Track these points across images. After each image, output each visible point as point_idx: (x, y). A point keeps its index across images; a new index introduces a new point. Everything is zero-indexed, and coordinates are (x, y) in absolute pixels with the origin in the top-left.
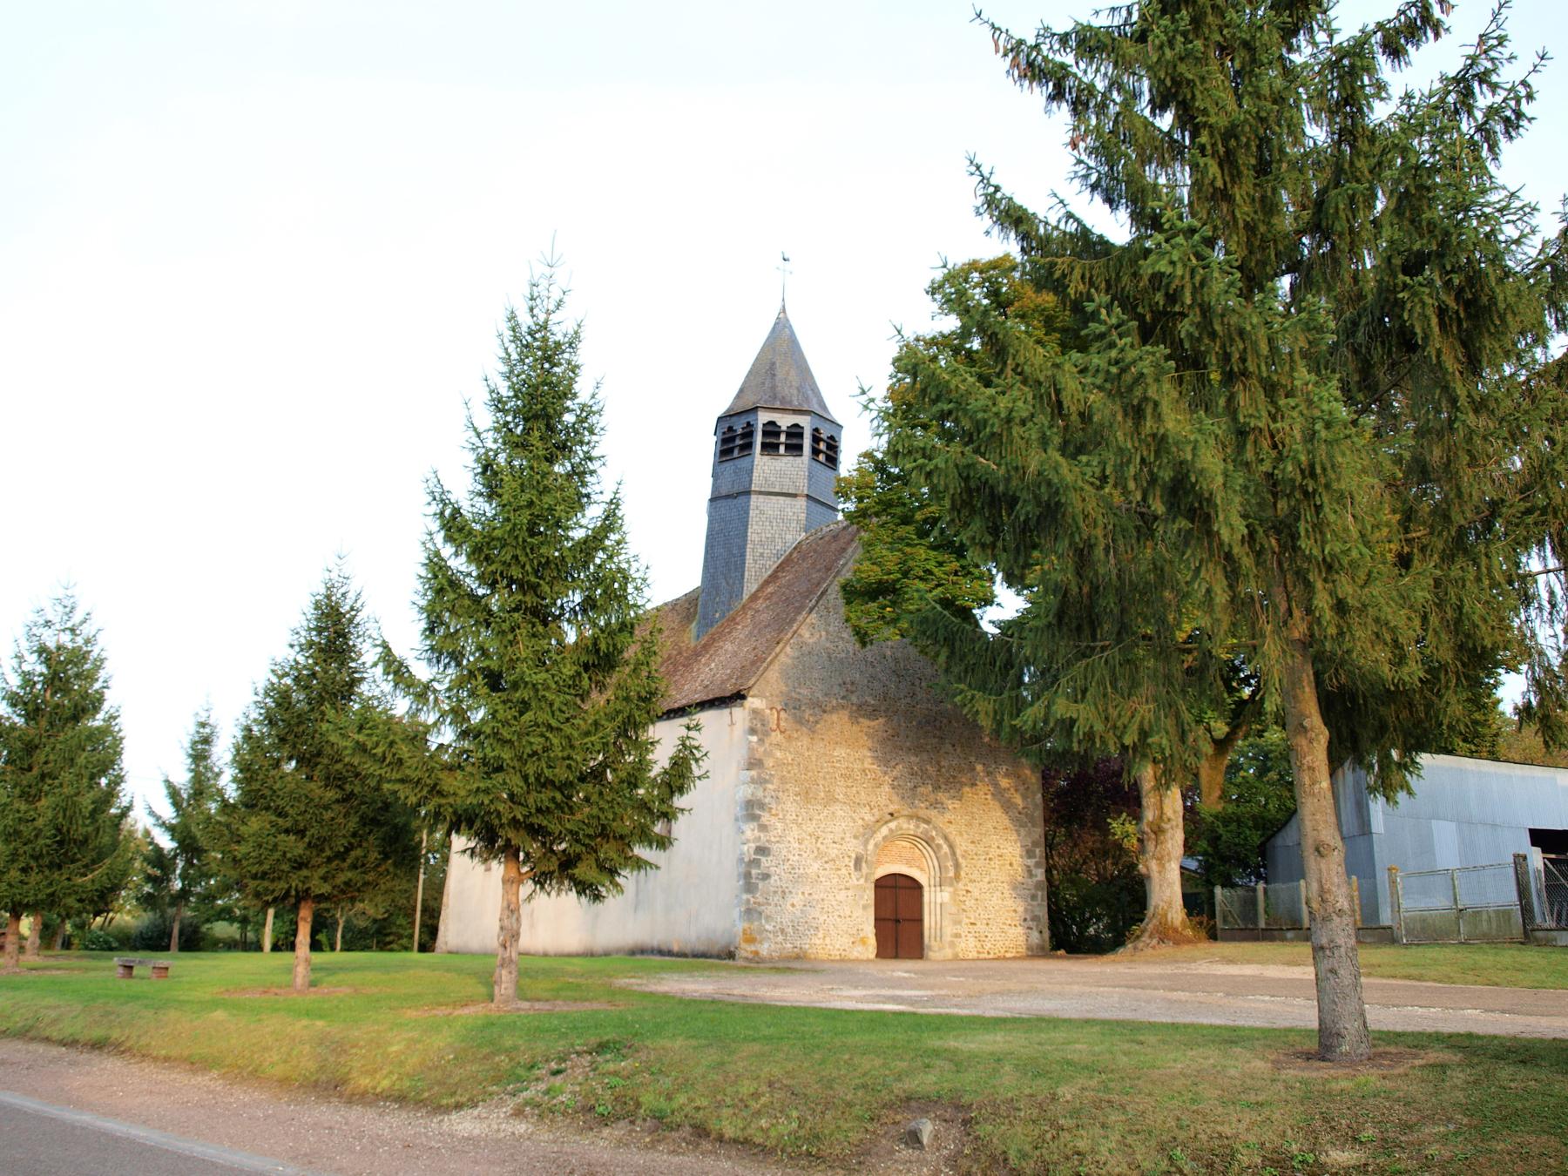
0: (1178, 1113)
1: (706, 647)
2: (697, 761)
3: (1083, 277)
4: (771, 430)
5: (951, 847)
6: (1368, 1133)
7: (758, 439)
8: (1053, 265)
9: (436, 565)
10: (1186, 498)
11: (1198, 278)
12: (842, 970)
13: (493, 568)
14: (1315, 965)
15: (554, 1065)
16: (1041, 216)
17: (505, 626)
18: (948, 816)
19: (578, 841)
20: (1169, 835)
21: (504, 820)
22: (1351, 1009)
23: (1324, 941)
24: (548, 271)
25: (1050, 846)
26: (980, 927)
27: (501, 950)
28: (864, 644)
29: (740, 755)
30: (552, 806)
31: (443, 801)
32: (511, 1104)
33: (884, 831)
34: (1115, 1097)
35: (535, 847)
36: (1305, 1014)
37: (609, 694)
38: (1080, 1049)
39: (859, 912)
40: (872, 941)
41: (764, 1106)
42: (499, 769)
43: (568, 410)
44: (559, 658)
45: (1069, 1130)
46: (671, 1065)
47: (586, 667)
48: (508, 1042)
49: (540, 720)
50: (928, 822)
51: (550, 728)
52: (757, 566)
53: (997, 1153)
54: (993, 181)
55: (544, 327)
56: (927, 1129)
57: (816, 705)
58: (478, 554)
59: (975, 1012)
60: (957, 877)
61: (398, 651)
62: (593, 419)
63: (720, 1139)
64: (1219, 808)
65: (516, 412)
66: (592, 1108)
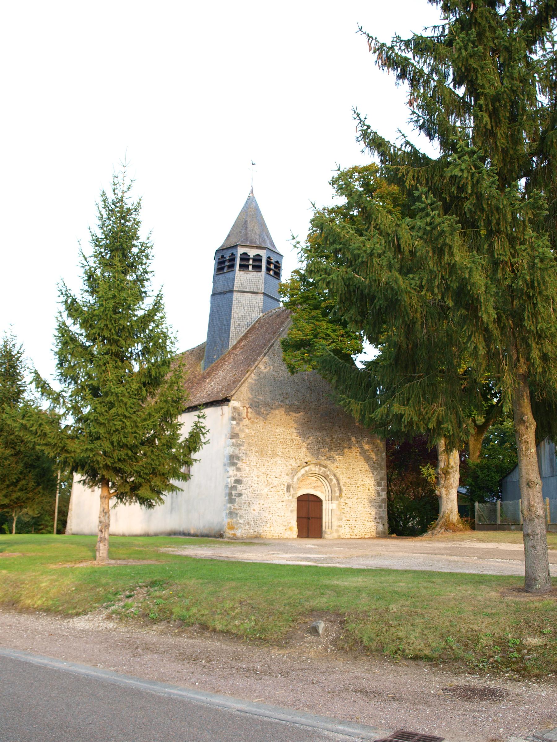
1: (209, 374)
3: (413, 177)
4: (245, 257)
5: (338, 480)
6: (548, 629)
7: (238, 262)
9: (63, 330)
10: (465, 298)
11: (475, 179)
12: (279, 544)
13: (94, 331)
15: (127, 593)
18: (336, 464)
19: (140, 476)
20: (452, 475)
21: (101, 465)
22: (542, 566)
23: (530, 531)
24: (123, 169)
26: (352, 522)
27: (99, 533)
28: (293, 373)
29: (226, 431)
30: (126, 458)
31: (68, 455)
32: (105, 613)
33: (303, 471)
34: (418, 610)
35: (117, 480)
36: (518, 568)
37: (157, 398)
38: (402, 585)
39: (288, 514)
40: (295, 529)
41: (237, 614)
42: (98, 438)
43: (134, 246)
44: (129, 379)
45: (395, 627)
47: (144, 384)
48: (104, 581)
49: (119, 413)
50: (325, 467)
51: (125, 417)
53: (358, 638)
54: (366, 123)
56: (321, 626)
57: (267, 405)
59: (348, 566)
60: (340, 496)
61: (43, 376)
62: (148, 251)
63: (214, 630)
64: (479, 461)
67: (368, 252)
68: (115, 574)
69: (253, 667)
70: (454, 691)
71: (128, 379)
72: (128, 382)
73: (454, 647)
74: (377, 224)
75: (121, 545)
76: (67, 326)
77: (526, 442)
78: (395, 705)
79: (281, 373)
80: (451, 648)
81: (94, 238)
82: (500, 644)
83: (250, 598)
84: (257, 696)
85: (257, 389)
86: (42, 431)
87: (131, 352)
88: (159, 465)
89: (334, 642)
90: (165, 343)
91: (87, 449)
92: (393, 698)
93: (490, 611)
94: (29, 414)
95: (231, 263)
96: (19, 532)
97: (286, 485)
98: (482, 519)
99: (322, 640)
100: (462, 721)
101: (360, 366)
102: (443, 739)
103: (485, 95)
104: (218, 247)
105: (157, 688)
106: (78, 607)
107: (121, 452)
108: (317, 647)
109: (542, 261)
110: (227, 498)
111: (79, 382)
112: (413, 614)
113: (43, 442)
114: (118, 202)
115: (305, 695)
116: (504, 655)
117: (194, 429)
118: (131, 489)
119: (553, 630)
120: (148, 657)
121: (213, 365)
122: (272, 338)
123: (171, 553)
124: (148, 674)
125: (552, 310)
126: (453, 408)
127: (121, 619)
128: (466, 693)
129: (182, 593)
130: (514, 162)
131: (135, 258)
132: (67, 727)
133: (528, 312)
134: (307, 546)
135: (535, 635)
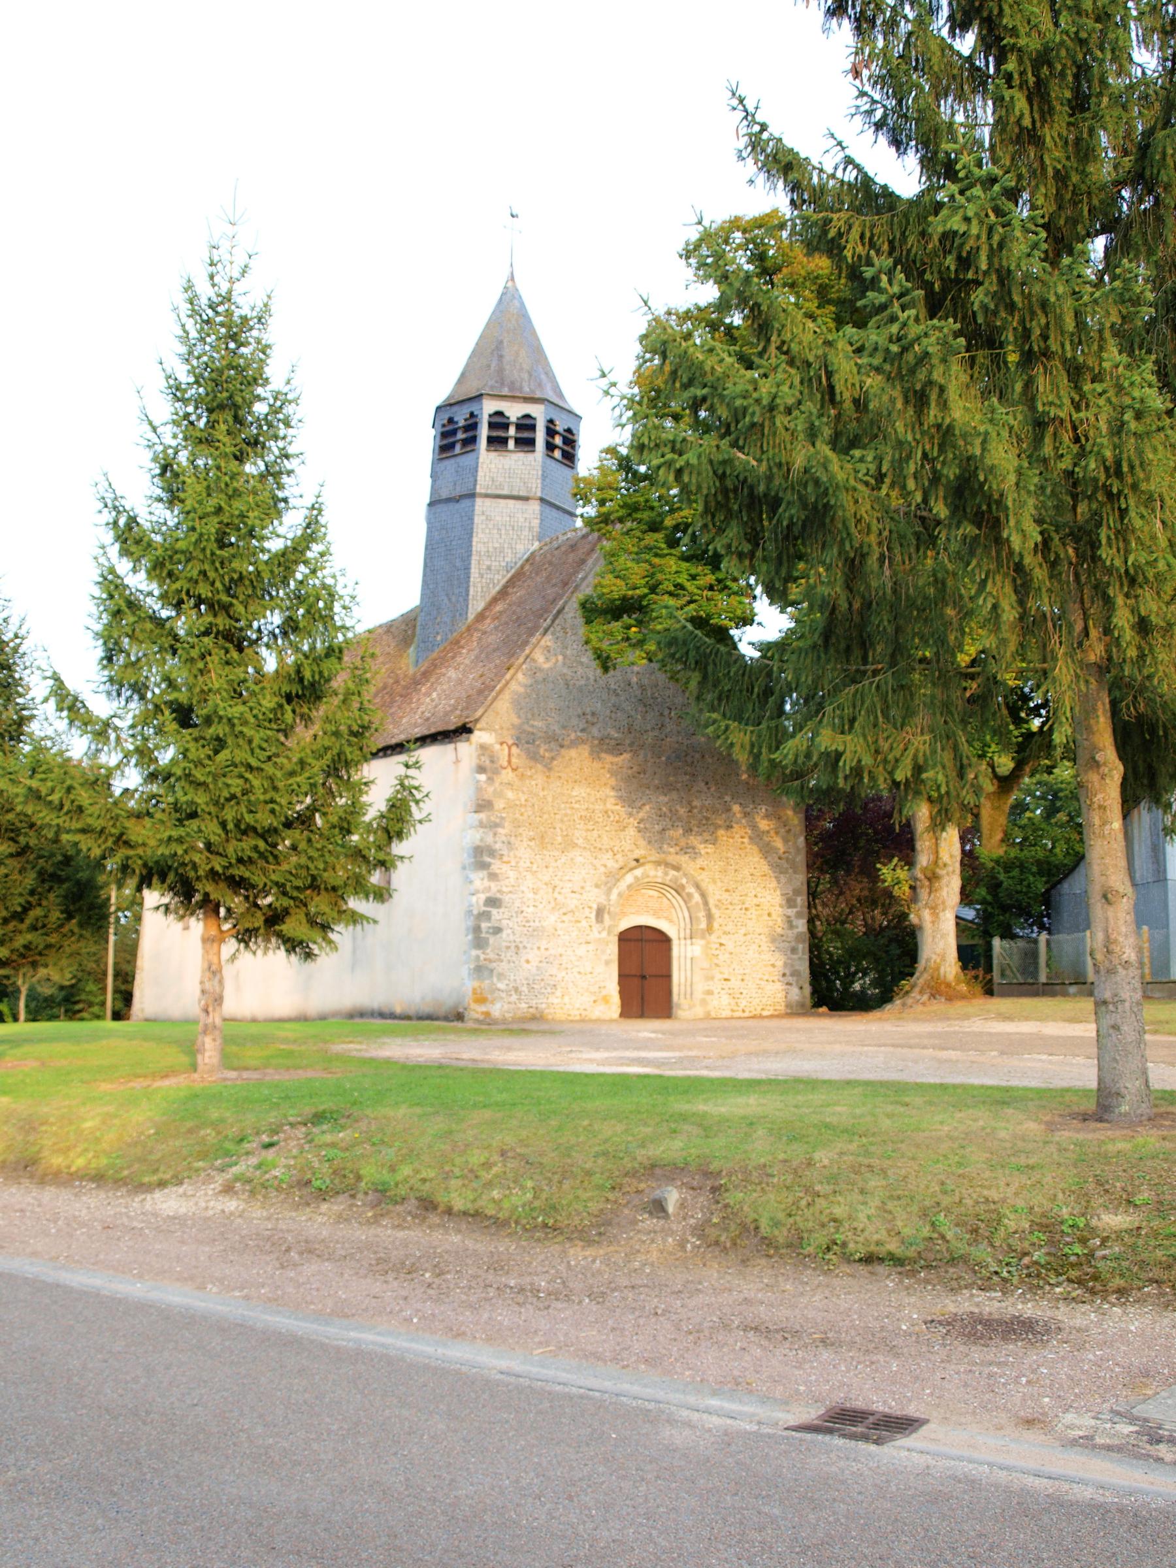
0: (943, 1177)
1: (426, 675)
3: (862, 237)
4: (499, 422)
5: (703, 895)
7: (484, 432)
8: (827, 222)
9: (112, 585)
10: (974, 501)
11: (996, 239)
12: (583, 1031)
13: (177, 585)
14: (1097, 1021)
15: (265, 1138)
16: (815, 162)
17: (195, 653)
18: (700, 862)
19: (285, 894)
20: (944, 881)
23: (1107, 995)
26: (735, 983)
27: (203, 1015)
28: (606, 669)
30: (255, 855)
31: (131, 853)
32: (220, 1180)
33: (629, 879)
34: (875, 1162)
35: (237, 902)
37: (316, 728)
38: (841, 1111)
41: (496, 1176)
42: (193, 815)
43: (259, 398)
44: (257, 688)
45: (825, 1197)
47: (289, 698)
48: (215, 1115)
50: (677, 868)
51: (250, 768)
52: (483, 582)
53: (748, 1220)
54: (758, 118)
55: (227, 298)
56: (673, 1197)
58: (161, 569)
60: (710, 929)
61: (71, 685)
62: (289, 409)
63: (449, 1211)
65: (197, 403)
69: (532, 1284)
70: (949, 1324)
72: (253, 694)
74: (783, 342)
75: (245, 1039)
77: (1102, 808)
78: (826, 1355)
79: (580, 670)
80: (943, 1237)
81: (172, 382)
82: (1044, 1227)
84: (540, 1343)
85: (529, 705)
87: (259, 630)
88: (325, 870)
89: (700, 1230)
90: (331, 609)
91: (170, 838)
92: (823, 1341)
93: (1023, 1161)
94: (44, 767)
95: (470, 434)
96: (33, 1017)
97: (595, 906)
98: (1008, 972)
100: (966, 1385)
103: (1020, 50)
104: (440, 400)
105: (332, 1330)
106: (162, 1168)
108: (664, 1240)
109: (1138, 416)
110: (470, 937)
111: (149, 695)
112: (863, 1169)
114: (222, 303)
116: (1053, 1250)
119: (1155, 1198)
120: (311, 1268)
124: (312, 1303)
127: (253, 1193)
129: (380, 1136)
130: (1081, 201)
131: (260, 426)
132: (148, 1413)
133: (1109, 528)
135: (1117, 1208)
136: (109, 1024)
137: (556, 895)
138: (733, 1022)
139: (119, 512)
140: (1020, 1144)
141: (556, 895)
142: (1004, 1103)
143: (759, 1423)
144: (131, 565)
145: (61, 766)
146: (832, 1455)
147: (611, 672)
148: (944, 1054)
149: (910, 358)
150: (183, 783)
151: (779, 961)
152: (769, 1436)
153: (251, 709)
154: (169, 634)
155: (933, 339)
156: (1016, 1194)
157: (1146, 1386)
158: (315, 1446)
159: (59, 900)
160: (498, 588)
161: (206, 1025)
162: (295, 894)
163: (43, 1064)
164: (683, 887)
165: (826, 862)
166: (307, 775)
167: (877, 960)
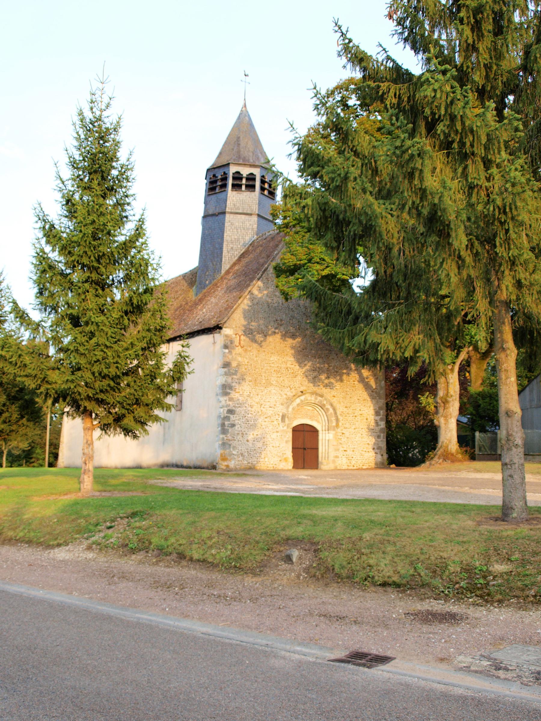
0: (422, 546)
1: (201, 300)
2: (188, 364)
3: (395, 95)
4: (238, 177)
5: (334, 409)
6: (516, 556)
7: (230, 182)
8: (379, 87)
9: (42, 257)
10: (436, 224)
11: (449, 99)
12: (274, 475)
13: (73, 258)
14: (502, 473)
15: (108, 524)
16: (374, 57)
17: (80, 291)
18: (333, 392)
19: (123, 407)
20: (451, 404)
21: (82, 397)
22: (519, 495)
23: (507, 461)
24: (101, 86)
25: (389, 408)
26: (349, 452)
27: (84, 465)
28: (287, 299)
29: (219, 362)
30: (108, 389)
31: (49, 386)
32: (86, 543)
33: (298, 401)
34: (391, 539)
35: (101, 411)
36: (494, 496)
37: (140, 327)
38: (380, 514)
41: (214, 543)
42: (79, 369)
43: (113, 167)
44: (110, 308)
45: (366, 555)
46: (168, 523)
47: (126, 313)
48: (85, 512)
49: (100, 343)
50: (322, 396)
51: (107, 347)
52: (230, 254)
53: (330, 566)
54: (348, 36)
55: (99, 119)
56: (295, 554)
58: (66, 250)
59: (335, 496)
60: (337, 426)
61: (22, 305)
62: (129, 173)
63: (191, 559)
64: (481, 389)
65: (84, 169)
66: (127, 545)
67: (342, 176)
68: (97, 506)
69: (224, 594)
70: (416, 615)
71: (109, 307)
72: (109, 310)
73: (422, 574)
74: (354, 146)
75: (104, 477)
76: (45, 253)
77: (506, 371)
78: (355, 628)
79: (275, 299)
80: (419, 575)
81: (72, 159)
82: (467, 571)
83: (228, 527)
84: (223, 620)
85: (250, 315)
86: (21, 362)
87: (113, 280)
88: (142, 396)
89: (307, 570)
90: (147, 270)
91: (67, 380)
92: (355, 622)
93: (461, 539)
94: (8, 345)
95: (223, 182)
96: (11, 464)
97: (281, 414)
98: (483, 449)
99: (295, 568)
100: (416, 642)
101: (357, 290)
102: (395, 658)
103: (467, 6)
105: (127, 613)
106: (59, 538)
107: (103, 383)
108: (290, 574)
109: (513, 185)
110: (220, 429)
111: (60, 310)
112: (385, 542)
113: (22, 373)
114: (96, 121)
115: (270, 619)
116: (470, 581)
117: (178, 359)
118: (114, 420)
119: (521, 558)
120: (123, 585)
121: (204, 291)
122: (265, 263)
123: (159, 484)
124: (121, 601)
125: (524, 236)
126: (431, 336)
127: (100, 550)
128: (427, 617)
129: (162, 523)
130: (498, 79)
131: (114, 182)
132: (35, 648)
133: (501, 238)
134: (300, 477)
135: (502, 562)
136: (46, 468)
137: (262, 408)
138: (347, 472)
139: (46, 222)
140: (461, 531)
141: (262, 408)
142: (460, 512)
143: (317, 658)
144: (51, 248)
145: (16, 345)
146: (347, 673)
147: (289, 301)
148: (443, 488)
149: (406, 156)
150: (74, 354)
151: (372, 440)
152: (319, 664)
153: (107, 318)
154: (69, 281)
155: (416, 148)
156: (455, 555)
157: (500, 644)
158: (109, 664)
159: (17, 409)
160: (236, 258)
161: (85, 470)
162: (128, 407)
163: (8, 488)
164: (324, 405)
165: (396, 394)
166: (134, 350)
167: (420, 442)
